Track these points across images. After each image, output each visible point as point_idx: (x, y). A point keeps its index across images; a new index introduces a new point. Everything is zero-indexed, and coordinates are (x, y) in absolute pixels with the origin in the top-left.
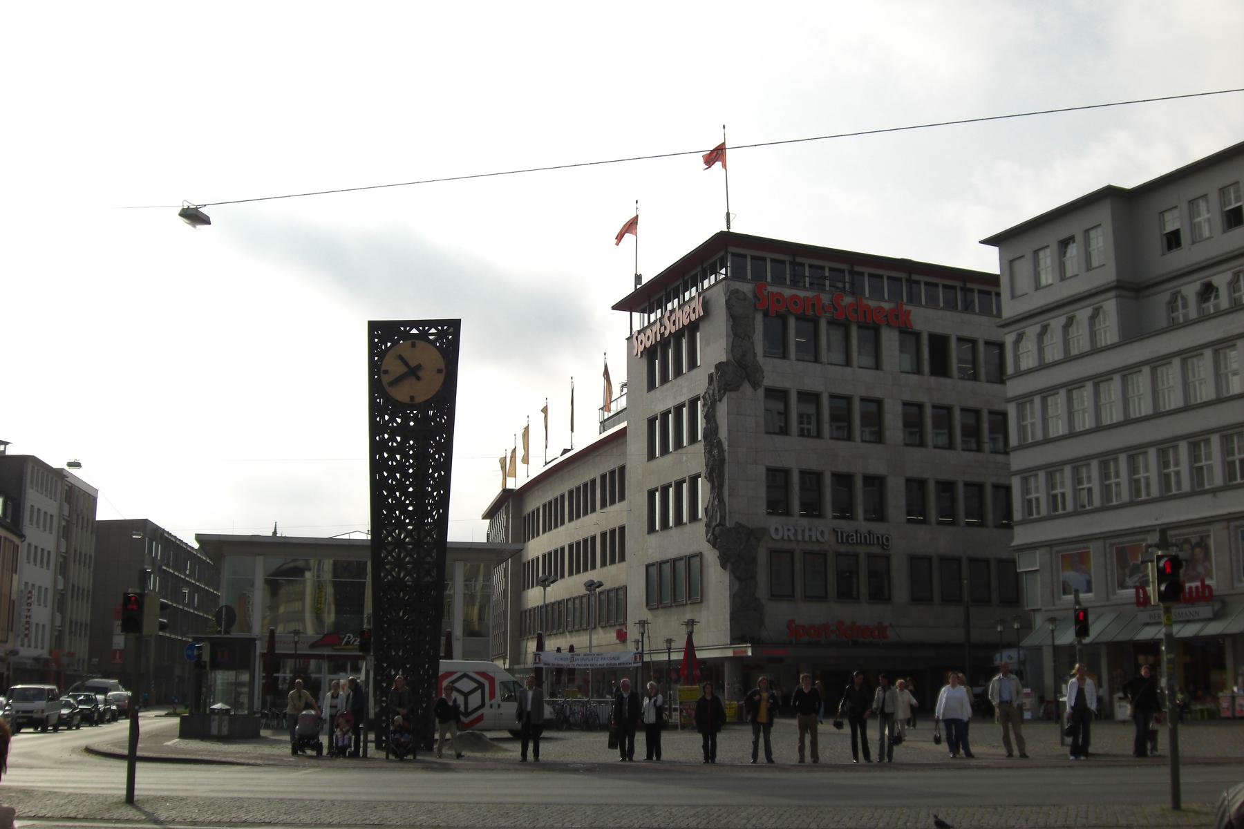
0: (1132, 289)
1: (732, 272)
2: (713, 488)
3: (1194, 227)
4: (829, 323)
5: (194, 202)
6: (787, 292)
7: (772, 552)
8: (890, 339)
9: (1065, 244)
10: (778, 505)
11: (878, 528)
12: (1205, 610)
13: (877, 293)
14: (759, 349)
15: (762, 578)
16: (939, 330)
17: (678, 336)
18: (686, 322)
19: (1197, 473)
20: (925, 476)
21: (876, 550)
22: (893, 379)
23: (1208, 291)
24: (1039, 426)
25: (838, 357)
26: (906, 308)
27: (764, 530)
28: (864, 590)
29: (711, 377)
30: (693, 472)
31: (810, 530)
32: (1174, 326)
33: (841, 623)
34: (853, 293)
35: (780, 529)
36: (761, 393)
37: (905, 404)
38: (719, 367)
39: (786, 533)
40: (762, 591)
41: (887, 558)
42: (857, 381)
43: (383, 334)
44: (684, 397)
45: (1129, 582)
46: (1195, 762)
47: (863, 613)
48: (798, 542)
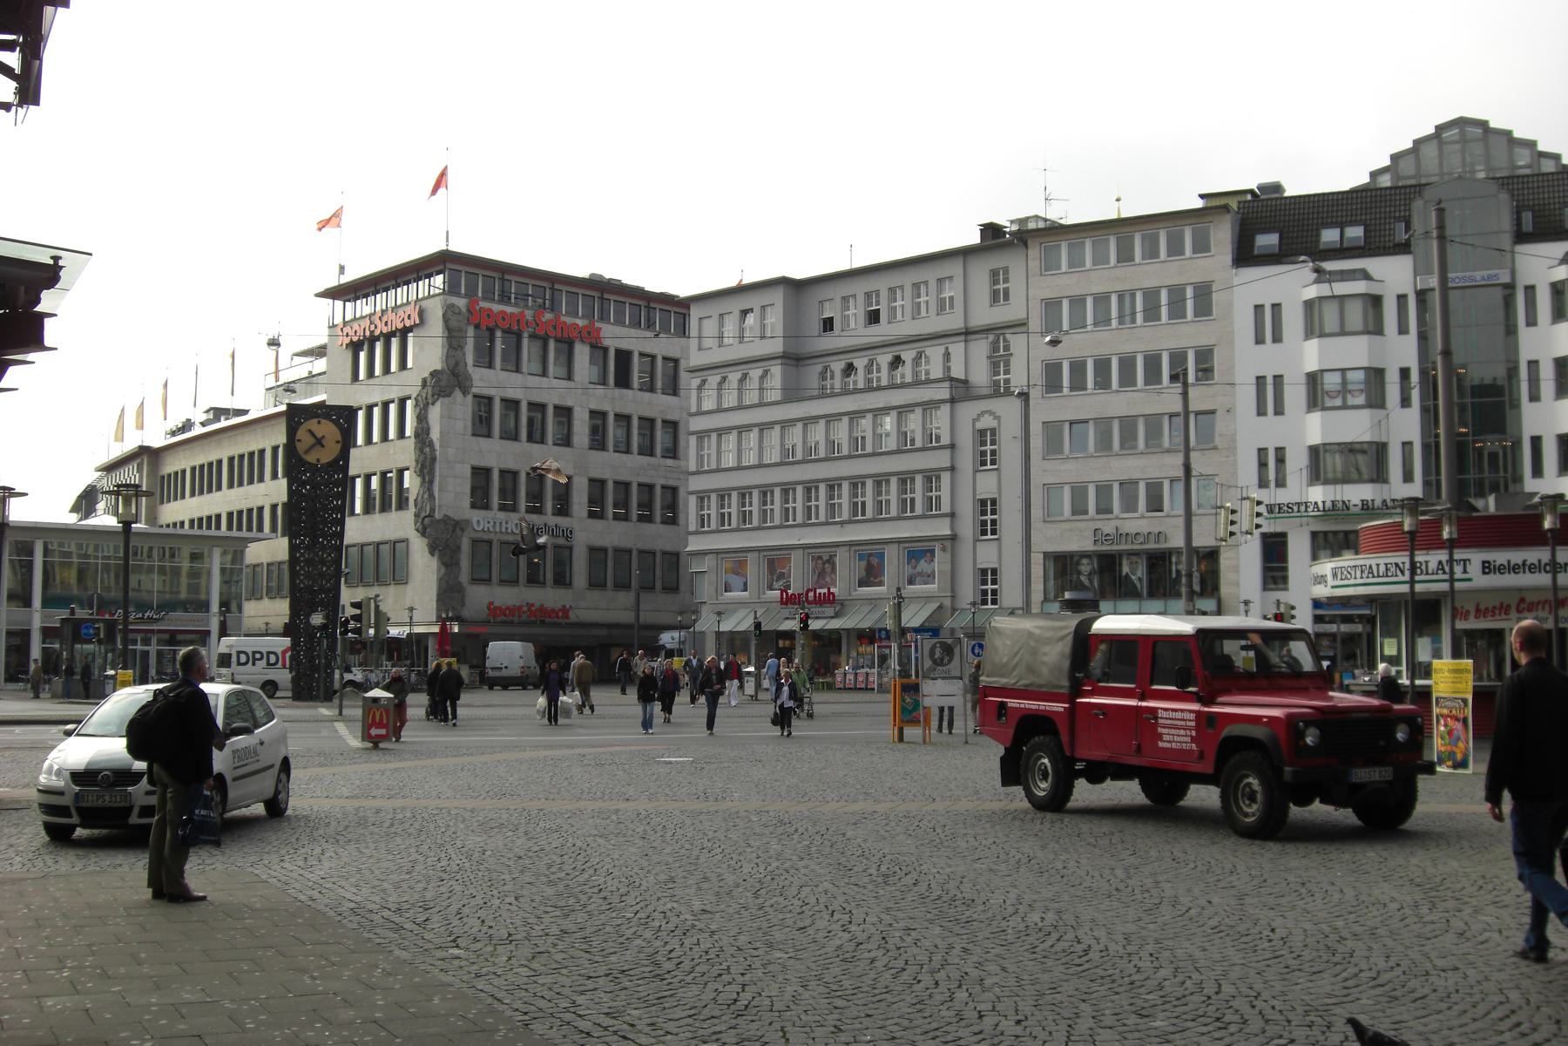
0: (794, 359)
2: (423, 482)
3: (846, 319)
6: (497, 308)
7: (475, 542)
8: (582, 353)
9: (745, 313)
10: (480, 498)
11: (562, 521)
12: (829, 611)
14: (470, 359)
15: (465, 563)
18: (400, 326)
19: (832, 508)
21: (561, 541)
22: (582, 390)
23: (850, 369)
24: (714, 457)
25: (537, 367)
26: (597, 325)
27: (468, 522)
28: (550, 576)
29: (424, 381)
30: (401, 466)
32: (823, 395)
33: (530, 605)
35: (482, 521)
36: (470, 397)
38: (434, 374)
40: (464, 577)
41: (571, 548)
42: (551, 391)
45: (776, 585)
46: (313, 446)
47: (549, 597)
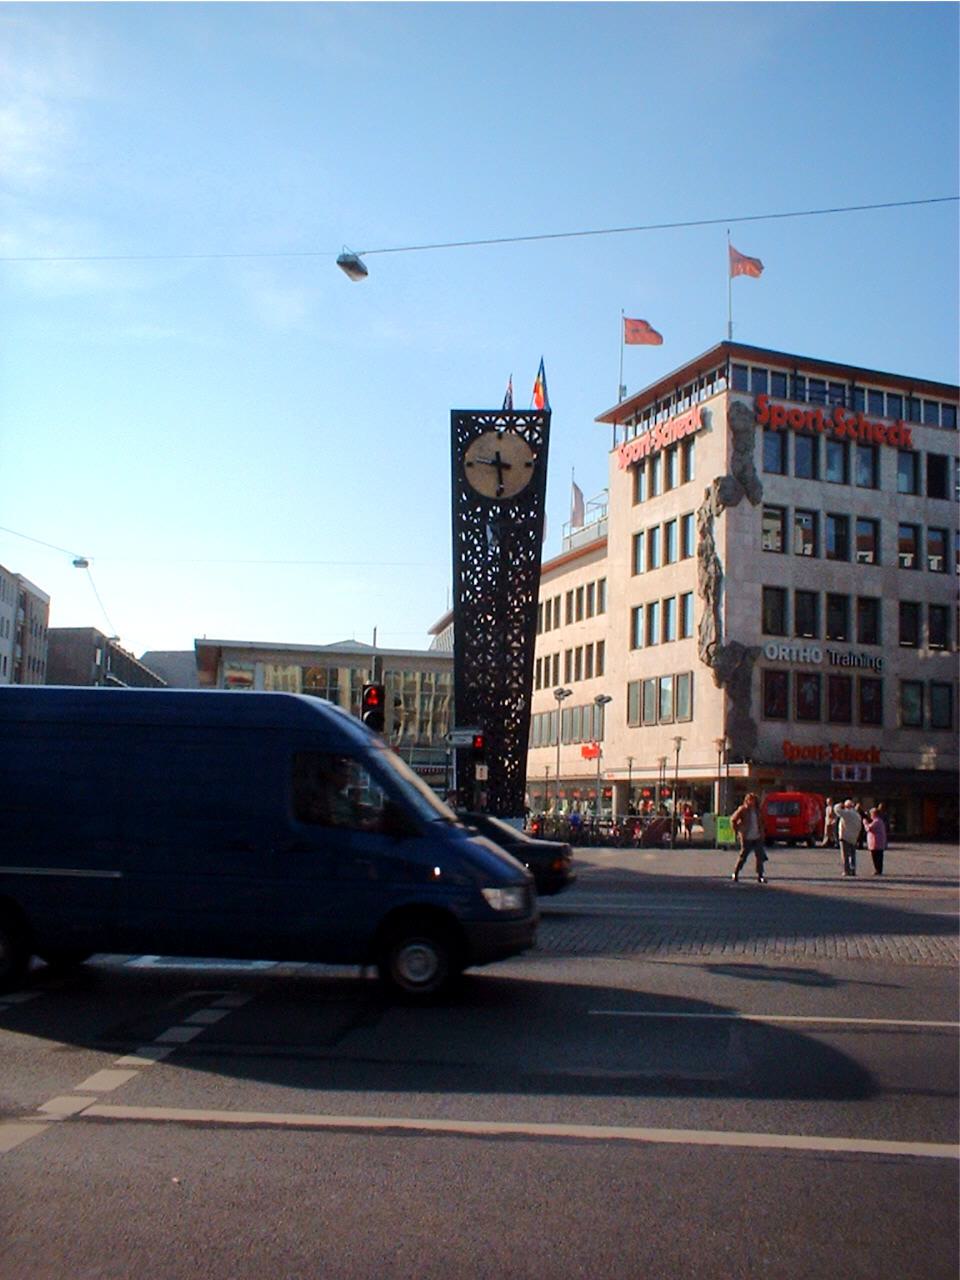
1: (733, 384)
4: (829, 439)
5: (352, 249)
6: (788, 406)
8: (889, 457)
10: (773, 624)
13: (877, 410)
14: (758, 464)
15: (756, 697)
16: (937, 451)
17: (670, 450)
20: (919, 600)
21: (869, 673)
25: (836, 474)
26: (907, 426)
27: (759, 649)
30: (684, 590)
31: (805, 651)
34: (852, 408)
36: (759, 508)
37: (902, 525)
39: (781, 653)
42: (854, 500)
43: (466, 426)
44: (676, 513)
48: (792, 662)
